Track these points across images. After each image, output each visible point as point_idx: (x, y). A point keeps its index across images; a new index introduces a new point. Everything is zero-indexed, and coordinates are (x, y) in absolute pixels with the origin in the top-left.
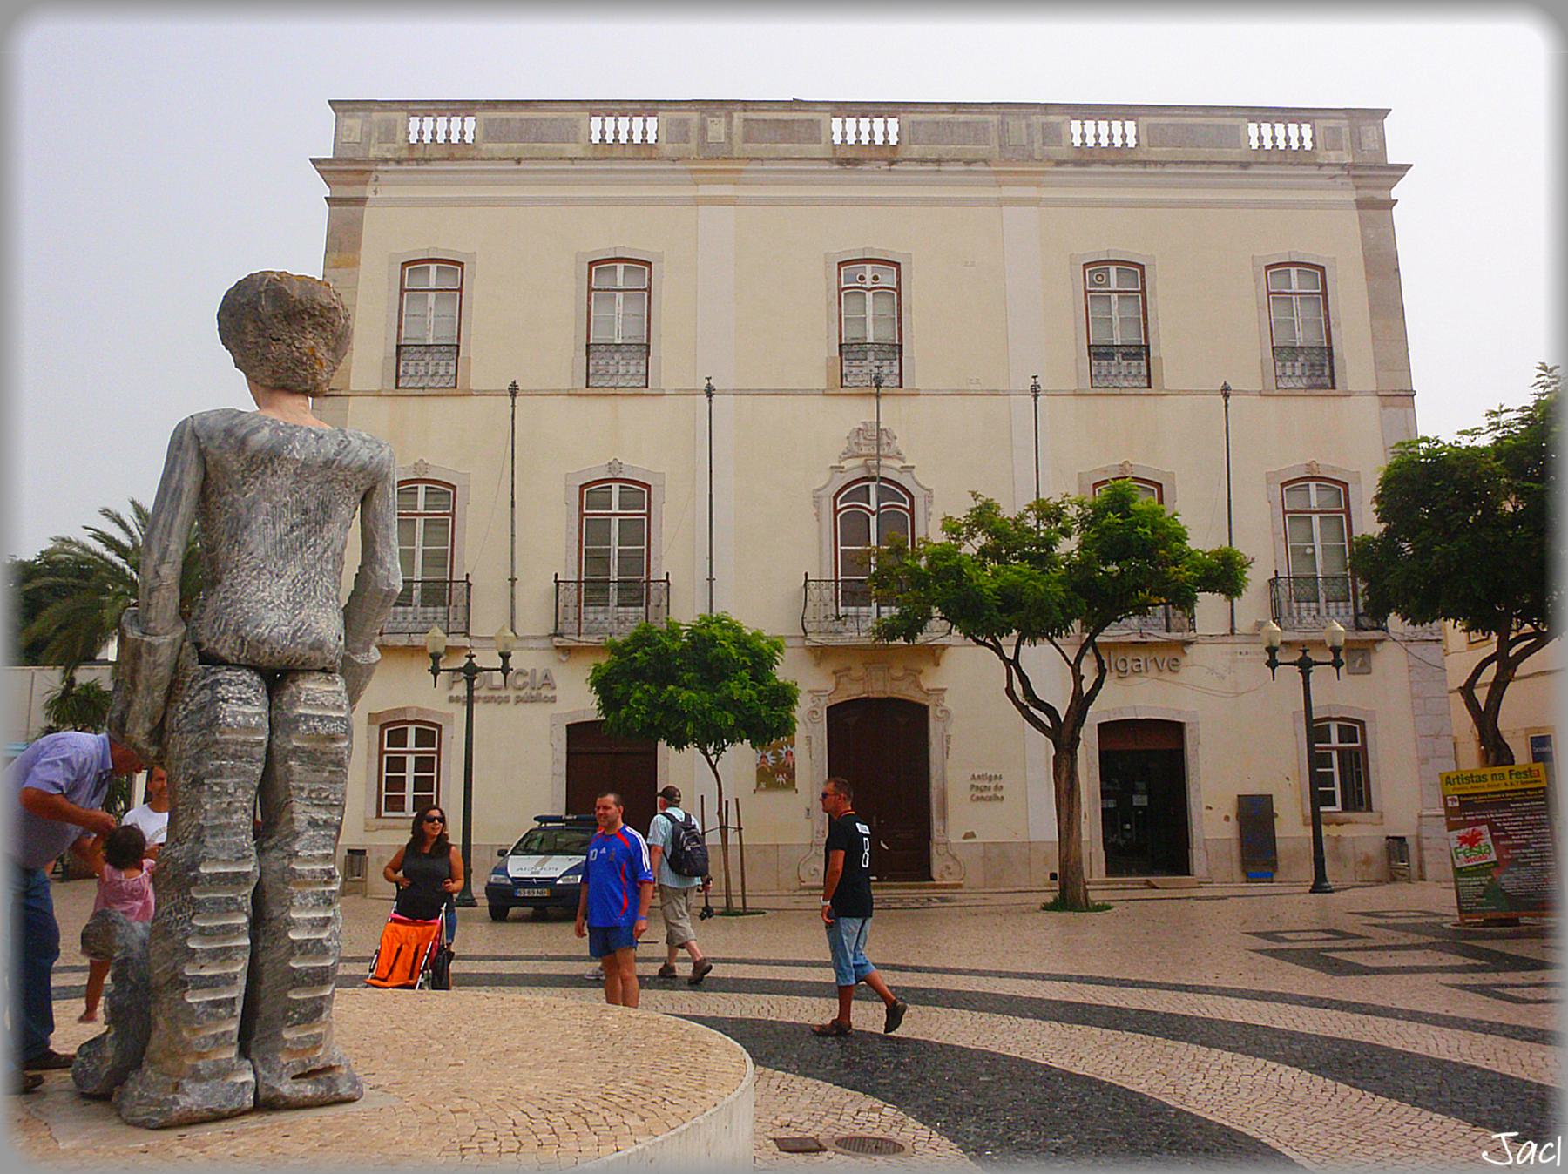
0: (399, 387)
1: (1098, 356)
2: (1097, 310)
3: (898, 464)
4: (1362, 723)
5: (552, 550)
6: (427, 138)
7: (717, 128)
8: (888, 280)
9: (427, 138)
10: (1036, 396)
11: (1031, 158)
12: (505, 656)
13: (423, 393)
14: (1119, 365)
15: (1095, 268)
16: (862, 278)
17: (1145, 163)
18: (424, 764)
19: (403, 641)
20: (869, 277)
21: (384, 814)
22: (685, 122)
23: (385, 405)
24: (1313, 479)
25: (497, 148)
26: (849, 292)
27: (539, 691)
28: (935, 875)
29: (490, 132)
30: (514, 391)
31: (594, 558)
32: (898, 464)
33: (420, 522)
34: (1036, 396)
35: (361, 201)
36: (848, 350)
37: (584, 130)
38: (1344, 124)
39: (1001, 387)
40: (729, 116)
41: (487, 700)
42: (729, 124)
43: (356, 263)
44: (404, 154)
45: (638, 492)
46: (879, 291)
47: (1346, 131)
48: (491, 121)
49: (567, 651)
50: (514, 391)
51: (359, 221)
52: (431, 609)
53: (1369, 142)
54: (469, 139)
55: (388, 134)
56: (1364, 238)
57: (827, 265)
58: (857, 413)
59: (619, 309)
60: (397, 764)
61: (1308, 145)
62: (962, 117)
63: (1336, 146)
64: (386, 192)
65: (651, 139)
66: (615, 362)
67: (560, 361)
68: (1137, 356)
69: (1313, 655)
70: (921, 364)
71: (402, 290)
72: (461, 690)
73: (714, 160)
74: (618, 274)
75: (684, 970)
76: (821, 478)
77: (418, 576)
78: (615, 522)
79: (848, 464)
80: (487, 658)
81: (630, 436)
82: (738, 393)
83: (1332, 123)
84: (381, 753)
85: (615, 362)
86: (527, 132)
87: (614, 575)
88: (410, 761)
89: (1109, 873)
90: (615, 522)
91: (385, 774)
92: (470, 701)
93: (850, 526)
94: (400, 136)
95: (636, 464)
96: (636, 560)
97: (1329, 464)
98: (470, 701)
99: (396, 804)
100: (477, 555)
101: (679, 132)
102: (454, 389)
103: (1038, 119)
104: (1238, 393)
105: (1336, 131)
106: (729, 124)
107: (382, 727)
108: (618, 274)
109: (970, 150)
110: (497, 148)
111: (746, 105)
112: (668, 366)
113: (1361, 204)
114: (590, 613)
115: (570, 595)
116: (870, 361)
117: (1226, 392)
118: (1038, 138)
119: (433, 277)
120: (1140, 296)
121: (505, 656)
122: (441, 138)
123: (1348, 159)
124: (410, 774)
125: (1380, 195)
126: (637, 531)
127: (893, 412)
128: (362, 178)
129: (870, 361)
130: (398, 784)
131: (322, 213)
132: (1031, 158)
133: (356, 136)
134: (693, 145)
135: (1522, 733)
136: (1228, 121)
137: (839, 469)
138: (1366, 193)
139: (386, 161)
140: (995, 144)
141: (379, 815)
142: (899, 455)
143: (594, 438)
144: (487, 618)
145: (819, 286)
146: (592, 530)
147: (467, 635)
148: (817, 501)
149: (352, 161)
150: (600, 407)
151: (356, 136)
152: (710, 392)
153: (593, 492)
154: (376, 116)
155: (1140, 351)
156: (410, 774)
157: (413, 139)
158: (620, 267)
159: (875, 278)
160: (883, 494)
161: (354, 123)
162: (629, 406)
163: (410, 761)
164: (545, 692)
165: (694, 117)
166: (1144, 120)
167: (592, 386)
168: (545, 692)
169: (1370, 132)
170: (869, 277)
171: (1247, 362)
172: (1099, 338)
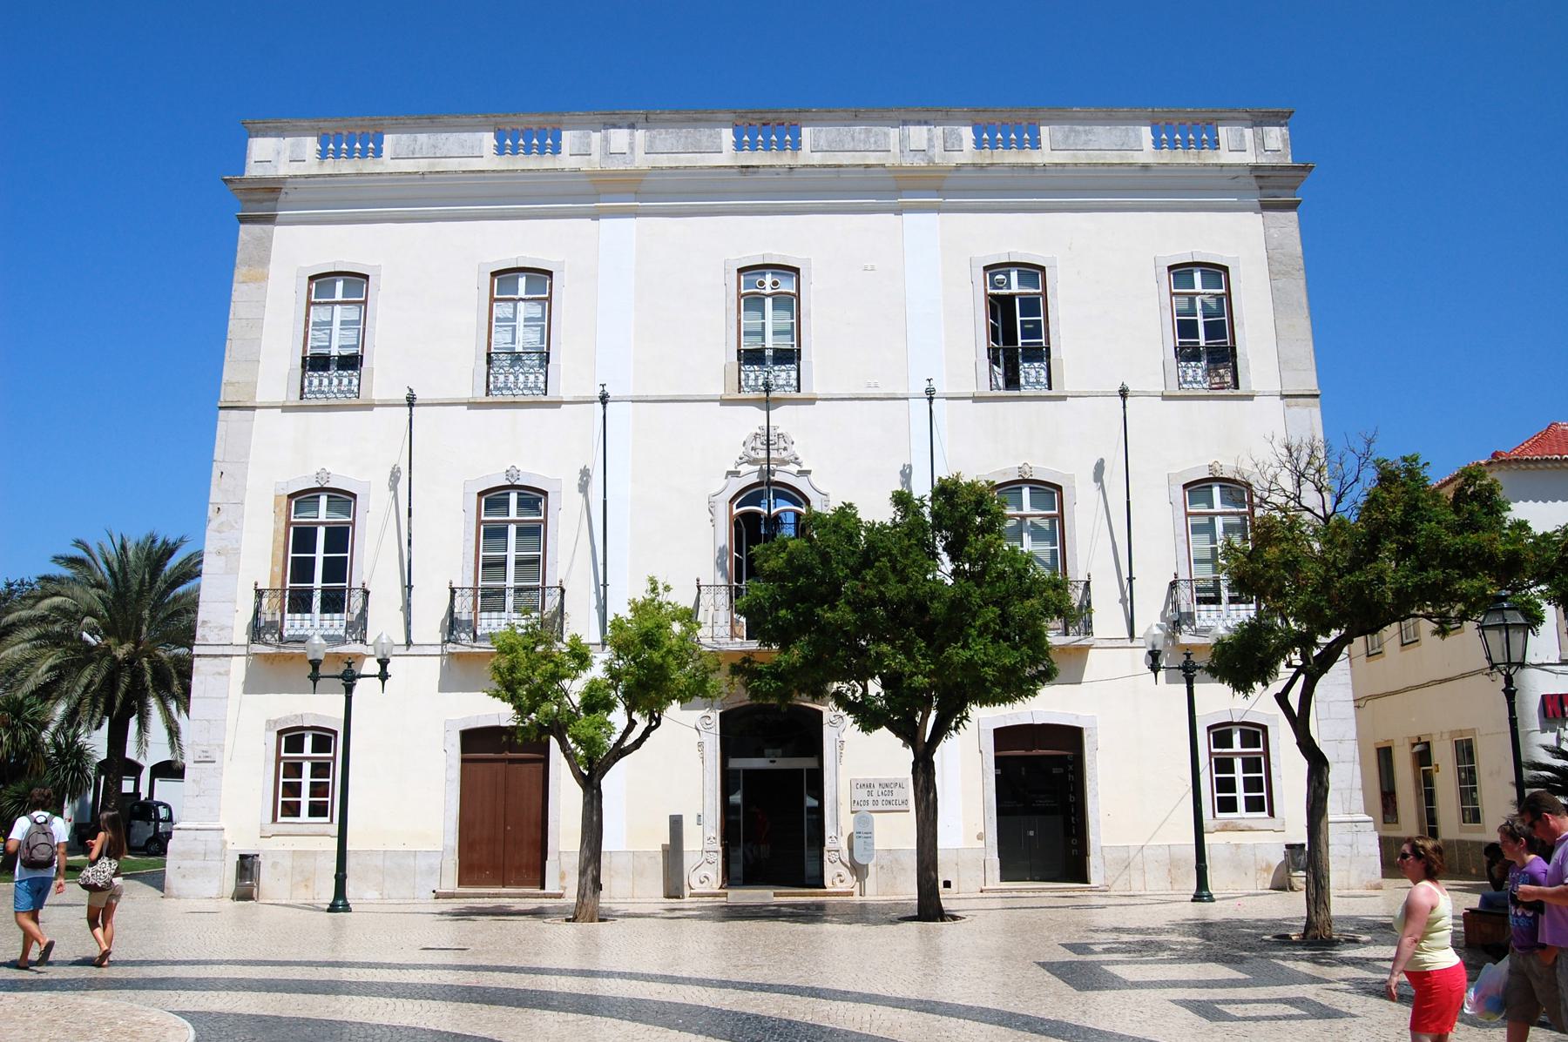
2: (750, 320)
3: (794, 468)
4: (1265, 728)
5: (448, 555)
8: (787, 287)
10: (931, 399)
16: (762, 284)
18: (320, 769)
20: (768, 286)
21: (280, 819)
24: (1216, 479)
28: (827, 882)
30: (411, 402)
32: (794, 468)
34: (931, 399)
36: (751, 357)
39: (900, 392)
43: (265, 278)
50: (411, 402)
52: (298, 616)
57: (726, 272)
58: (753, 418)
66: (516, 372)
68: (315, 358)
69: (403, 650)
70: (817, 369)
75: (34, 954)
76: (719, 483)
77: (288, 585)
78: (321, 532)
84: (279, 759)
85: (516, 372)
87: (511, 582)
88: (307, 767)
89: (1003, 878)
91: (282, 780)
96: (337, 569)
97: (530, 476)
107: (280, 733)
112: (567, 376)
116: (769, 363)
117: (1124, 393)
120: (789, 303)
124: (306, 780)
126: (339, 538)
127: (782, 418)
128: (273, 196)
129: (769, 363)
130: (294, 790)
135: (1446, 736)
137: (736, 474)
141: (275, 819)
145: (721, 294)
152: (604, 399)
156: (306, 780)
159: (775, 283)
163: (307, 767)
170: (768, 286)
172: (315, 346)
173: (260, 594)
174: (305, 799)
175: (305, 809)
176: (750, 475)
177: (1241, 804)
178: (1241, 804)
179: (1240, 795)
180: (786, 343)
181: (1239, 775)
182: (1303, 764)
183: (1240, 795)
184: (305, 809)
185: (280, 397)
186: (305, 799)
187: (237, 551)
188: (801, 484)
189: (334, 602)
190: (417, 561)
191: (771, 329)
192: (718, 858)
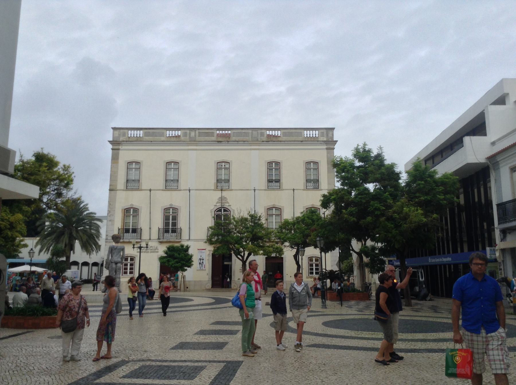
0: (127, 189)
1: (270, 182)
3: (228, 204)
5: (158, 222)
6: (132, 135)
7: (193, 134)
8: (227, 166)
9: (132, 135)
11: (257, 140)
12: (147, 245)
13: (132, 190)
14: (274, 184)
15: (270, 163)
17: (281, 141)
18: (132, 265)
19: (127, 241)
20: (223, 166)
22: (186, 133)
23: (124, 192)
25: (147, 138)
26: (218, 169)
27: (155, 250)
29: (146, 134)
31: (167, 224)
32: (228, 204)
33: (131, 216)
35: (119, 149)
37: (165, 134)
38: (325, 131)
40: (195, 131)
41: (145, 252)
42: (195, 133)
44: (128, 139)
45: (175, 210)
46: (225, 168)
47: (325, 133)
48: (146, 132)
49: (161, 242)
51: (118, 154)
53: (330, 135)
54: (141, 136)
55: (124, 135)
56: (327, 156)
58: (218, 194)
59: (172, 172)
60: (311, 265)
61: (317, 136)
62: (244, 131)
63: (323, 136)
64: (124, 147)
65: (141, 136)
66: (171, 183)
67: (160, 183)
68: (278, 182)
70: (234, 183)
71: (128, 168)
72: (139, 250)
73: (193, 141)
74: (172, 165)
78: (171, 216)
79: (218, 204)
80: (143, 244)
81: (175, 199)
82: (184, 190)
83: (322, 131)
85: (171, 183)
86: (153, 135)
88: (129, 264)
90: (171, 216)
92: (140, 252)
93: (217, 217)
94: (127, 135)
95: (176, 204)
96: (174, 224)
97: (278, 205)
98: (140, 252)
99: (312, 273)
100: (143, 224)
101: (185, 135)
102: (138, 189)
103: (259, 131)
104: (297, 189)
105: (323, 133)
106: (195, 133)
108: (172, 165)
109: (245, 138)
110: (147, 138)
111: (199, 129)
112: (183, 184)
113: (327, 149)
114: (166, 234)
115: (161, 231)
116: (222, 183)
118: (259, 135)
119: (134, 166)
121: (147, 245)
122: (135, 135)
123: (325, 139)
124: (129, 267)
125: (332, 147)
126: (175, 218)
127: (225, 194)
129: (222, 183)
130: (312, 269)
131: (110, 152)
132: (257, 140)
133: (117, 135)
134: (188, 137)
136: (300, 131)
138: (328, 146)
139: (124, 141)
140: (250, 137)
142: (228, 203)
143: (167, 199)
144: (145, 236)
146: (166, 218)
147: (141, 239)
148: (211, 212)
149: (116, 141)
150: (168, 193)
151: (117, 135)
152: (255, 190)
153: (166, 210)
154: (122, 131)
155: (278, 181)
156: (129, 267)
157: (129, 136)
158: (173, 163)
160: (225, 211)
161: (117, 132)
162: (174, 193)
163: (129, 264)
164: (156, 250)
165: (188, 131)
166: (282, 131)
167: (166, 188)
168: (156, 250)
169: (330, 133)
170: (223, 166)
171: (301, 183)
173: (119, 229)
174: (128, 271)
175: (128, 273)
176: (219, 205)
177: (314, 273)
178: (314, 273)
179: (314, 271)
180: (227, 178)
181: (314, 267)
182: (296, 266)
183: (314, 271)
184: (128, 273)
185: (122, 188)
186: (128, 271)
187: (114, 220)
188: (229, 208)
189: (174, 231)
190: (151, 223)
191: (172, 175)
192: (211, 282)
